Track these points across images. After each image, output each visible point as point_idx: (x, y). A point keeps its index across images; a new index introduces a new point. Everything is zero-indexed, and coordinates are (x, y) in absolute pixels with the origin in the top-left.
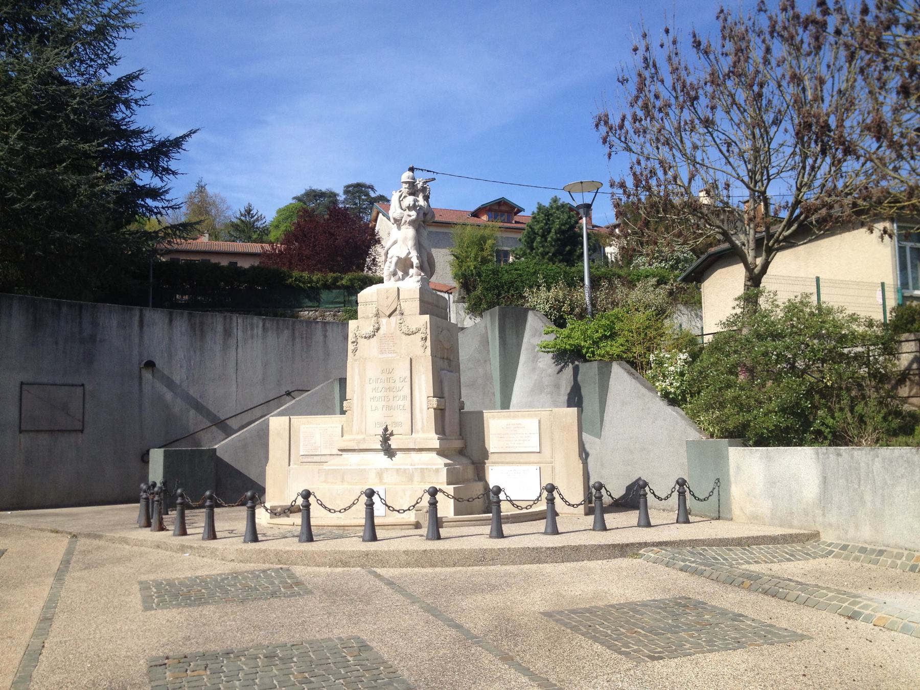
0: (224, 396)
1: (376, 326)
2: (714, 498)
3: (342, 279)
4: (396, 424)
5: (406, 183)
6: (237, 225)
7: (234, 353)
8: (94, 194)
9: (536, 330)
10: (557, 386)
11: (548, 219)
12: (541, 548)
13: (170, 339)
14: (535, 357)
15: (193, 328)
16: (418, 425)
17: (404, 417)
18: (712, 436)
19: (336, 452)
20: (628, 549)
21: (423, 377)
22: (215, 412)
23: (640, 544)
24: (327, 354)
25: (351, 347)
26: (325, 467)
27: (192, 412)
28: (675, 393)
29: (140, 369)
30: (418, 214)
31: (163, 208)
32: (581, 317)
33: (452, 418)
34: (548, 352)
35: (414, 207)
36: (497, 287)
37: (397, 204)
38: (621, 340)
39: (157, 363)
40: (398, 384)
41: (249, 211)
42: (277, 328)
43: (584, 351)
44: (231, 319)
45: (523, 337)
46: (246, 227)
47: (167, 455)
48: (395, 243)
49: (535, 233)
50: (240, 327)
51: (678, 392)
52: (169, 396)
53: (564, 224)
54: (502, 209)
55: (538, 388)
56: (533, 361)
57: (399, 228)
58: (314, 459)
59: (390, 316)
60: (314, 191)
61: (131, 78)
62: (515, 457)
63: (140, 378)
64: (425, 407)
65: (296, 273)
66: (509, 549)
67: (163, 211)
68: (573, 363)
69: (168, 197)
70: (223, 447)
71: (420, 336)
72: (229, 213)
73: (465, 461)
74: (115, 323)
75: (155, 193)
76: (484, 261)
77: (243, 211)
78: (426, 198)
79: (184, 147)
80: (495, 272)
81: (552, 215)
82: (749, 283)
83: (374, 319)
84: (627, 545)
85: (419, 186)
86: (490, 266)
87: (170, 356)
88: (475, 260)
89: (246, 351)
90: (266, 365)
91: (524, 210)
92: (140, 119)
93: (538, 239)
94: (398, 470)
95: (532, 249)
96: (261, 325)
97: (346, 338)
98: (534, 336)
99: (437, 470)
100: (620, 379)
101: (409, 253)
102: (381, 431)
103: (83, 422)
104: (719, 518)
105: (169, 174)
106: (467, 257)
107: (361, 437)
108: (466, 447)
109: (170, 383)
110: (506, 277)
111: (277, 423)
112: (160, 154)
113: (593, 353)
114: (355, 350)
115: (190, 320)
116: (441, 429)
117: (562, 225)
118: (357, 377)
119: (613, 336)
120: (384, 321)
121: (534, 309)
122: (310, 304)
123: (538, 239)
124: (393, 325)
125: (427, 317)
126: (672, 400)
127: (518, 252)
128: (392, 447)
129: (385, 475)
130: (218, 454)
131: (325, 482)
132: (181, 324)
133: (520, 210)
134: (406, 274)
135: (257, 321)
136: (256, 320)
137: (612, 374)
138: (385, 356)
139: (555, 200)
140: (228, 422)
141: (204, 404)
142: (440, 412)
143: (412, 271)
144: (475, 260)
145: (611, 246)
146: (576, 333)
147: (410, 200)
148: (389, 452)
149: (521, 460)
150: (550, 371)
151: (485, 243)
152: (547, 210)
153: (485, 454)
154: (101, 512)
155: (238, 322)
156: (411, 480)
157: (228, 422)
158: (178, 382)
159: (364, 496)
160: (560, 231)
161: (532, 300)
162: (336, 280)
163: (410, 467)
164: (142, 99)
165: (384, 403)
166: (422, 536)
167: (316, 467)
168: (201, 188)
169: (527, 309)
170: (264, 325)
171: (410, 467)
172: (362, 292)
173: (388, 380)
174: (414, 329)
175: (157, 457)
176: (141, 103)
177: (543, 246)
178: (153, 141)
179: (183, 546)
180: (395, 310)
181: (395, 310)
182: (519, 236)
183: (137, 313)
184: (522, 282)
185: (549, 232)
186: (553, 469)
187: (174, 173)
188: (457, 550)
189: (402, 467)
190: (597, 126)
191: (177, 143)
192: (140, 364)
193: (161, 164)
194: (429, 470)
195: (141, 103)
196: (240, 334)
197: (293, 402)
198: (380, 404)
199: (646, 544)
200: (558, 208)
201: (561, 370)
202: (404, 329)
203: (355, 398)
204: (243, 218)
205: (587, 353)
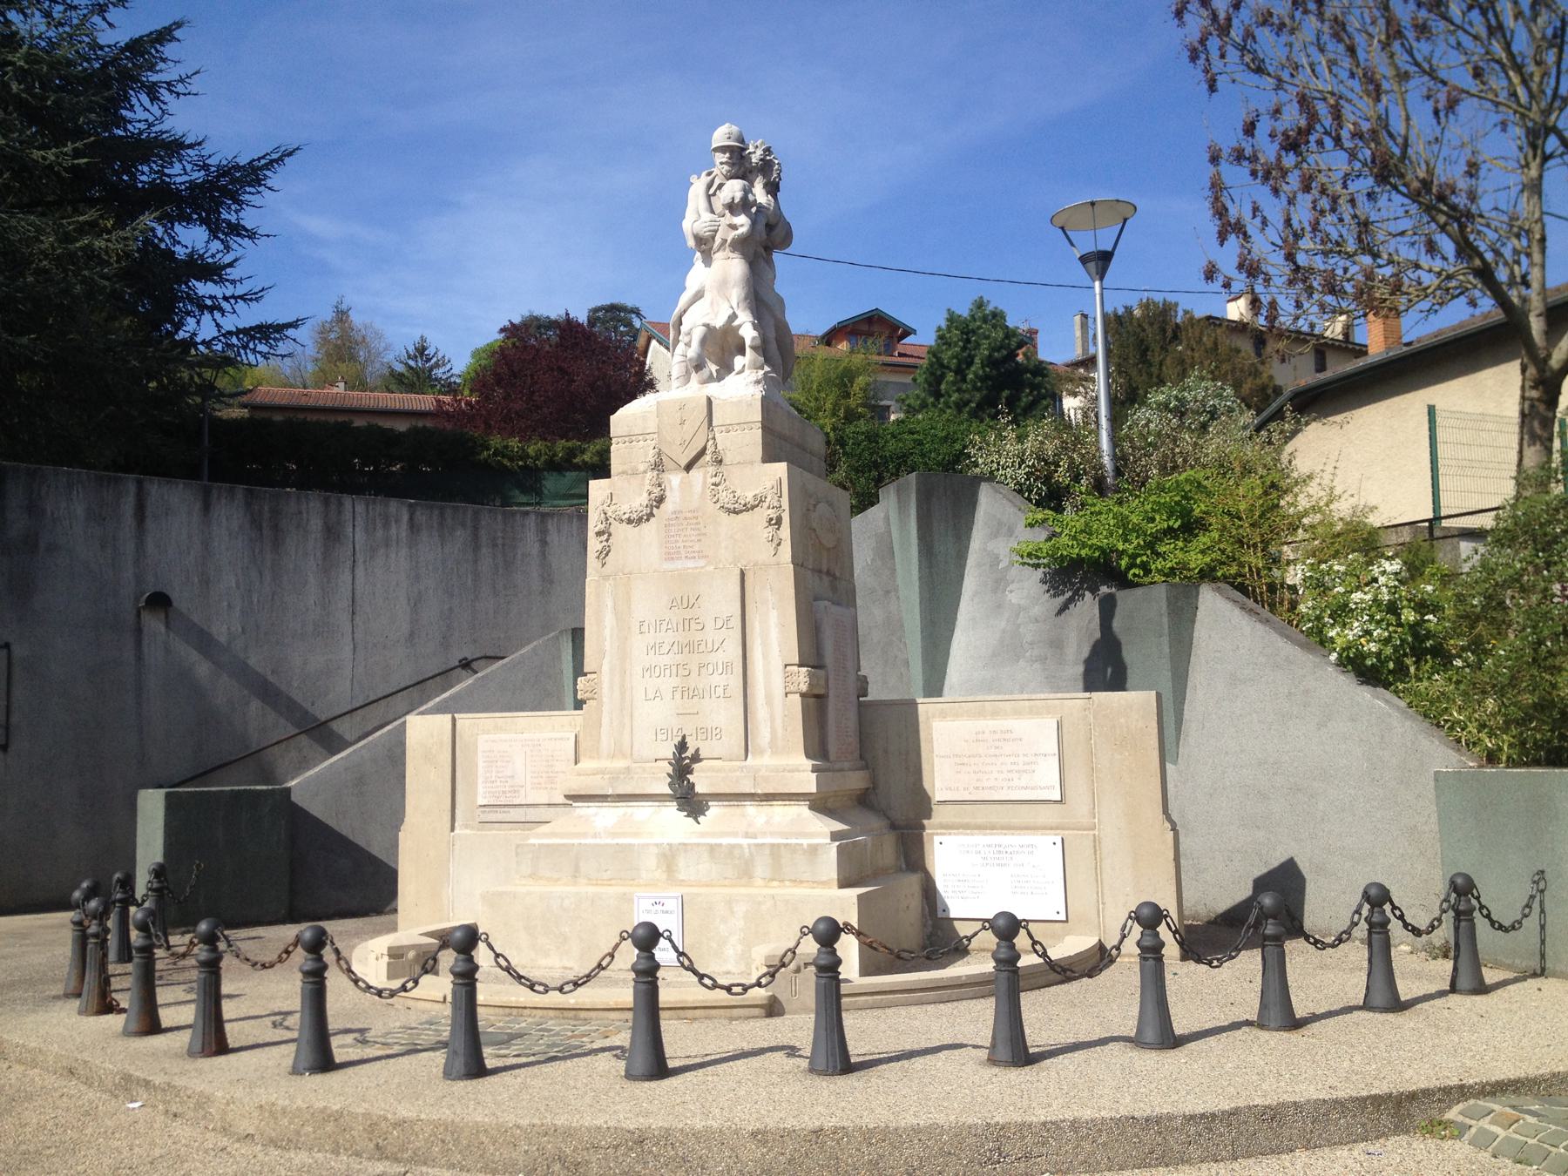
0: (327, 670)
1: (657, 491)
2: (1532, 923)
3: (583, 452)
4: (706, 733)
5: (723, 149)
6: (401, 375)
7: (347, 577)
8: (71, 256)
9: (1000, 524)
10: (1057, 644)
11: (968, 341)
12: (1171, 1117)
13: (206, 544)
14: (998, 581)
15: (256, 523)
16: (763, 734)
17: (725, 716)
18: (1492, 758)
19: (562, 800)
20: (1414, 1109)
21: (773, 616)
22: (307, 705)
23: (1447, 1091)
24: (548, 579)
25: (594, 545)
26: (536, 838)
27: (255, 705)
28: (1378, 654)
29: (138, 615)
30: (754, 223)
31: (225, 298)
32: (1099, 487)
33: (842, 720)
34: (1036, 566)
35: (742, 205)
36: (876, 465)
37: (703, 203)
38: (1204, 540)
39: (175, 596)
40: (711, 635)
41: (421, 350)
42: (441, 525)
43: (1123, 563)
44: (340, 504)
45: (969, 538)
46: (419, 372)
47: (172, 805)
48: (699, 296)
49: (942, 366)
50: (359, 521)
51: (1389, 650)
52: (203, 669)
53: (999, 349)
54: (875, 328)
55: (1009, 650)
56: (995, 591)
57: (708, 261)
58: (510, 815)
59: (688, 468)
60: (537, 318)
61: (164, 35)
62: (997, 814)
63: (139, 630)
64: (779, 691)
65: (496, 441)
66: (1075, 1125)
67: (225, 305)
68: (1094, 590)
69: (233, 273)
70: (311, 782)
71: (763, 513)
72: (389, 357)
73: (876, 823)
74: (80, 510)
75: (213, 272)
76: (851, 416)
77: (411, 350)
78: (773, 188)
79: (269, 183)
80: (872, 437)
81: (973, 332)
82: (1534, 394)
83: (649, 475)
84: (1412, 1096)
85: (755, 159)
86: (862, 426)
87: (206, 582)
88: (834, 414)
89: (383, 571)
90: (416, 603)
91: (914, 332)
92: (180, 119)
93: (950, 377)
94: (712, 849)
95: (938, 395)
96: (405, 518)
97: (583, 518)
98: (994, 535)
99: (814, 850)
100: (1219, 619)
101: (734, 317)
102: (669, 751)
103: (7, 728)
104: (1541, 973)
105: (243, 237)
106: (819, 409)
107: (620, 764)
108: (874, 781)
109: (204, 642)
110: (892, 445)
111: (424, 730)
112: (222, 192)
113: (1145, 568)
114: (605, 553)
115: (248, 505)
116: (817, 746)
117: (994, 350)
118: (609, 620)
119: (1190, 527)
120: (674, 480)
121: (991, 477)
122: (524, 499)
123: (950, 377)
124: (698, 488)
125: (781, 468)
126: (1366, 671)
127: (911, 401)
128: (699, 789)
129: (681, 862)
130: (293, 798)
131: (533, 876)
132: (230, 514)
133: (908, 332)
134: (726, 368)
135: (398, 509)
136: (394, 505)
137: (1200, 614)
138: (679, 565)
139: (980, 305)
140: (335, 725)
141: (283, 688)
142: (816, 705)
143: (739, 361)
144: (834, 414)
145: (1075, 395)
146: (1091, 525)
147: (734, 189)
148: (691, 802)
149: (1015, 821)
150: (1036, 610)
151: (852, 383)
152: (966, 323)
153: (922, 805)
154: (23, 935)
155: (355, 510)
156: (746, 874)
157: (335, 725)
158: (223, 639)
159: (628, 945)
160: (990, 362)
161: (983, 462)
162: (571, 453)
163: (744, 842)
164: (182, 80)
165: (675, 681)
166: (792, 1051)
167: (516, 834)
168: (342, 315)
169: (979, 479)
170: (411, 519)
171: (744, 842)
172: (622, 412)
173: (686, 623)
174: (749, 496)
175: (151, 806)
176: (180, 88)
177: (959, 390)
178: (205, 167)
179: (127, 1078)
180: (702, 452)
181: (702, 452)
182: (908, 379)
183: (132, 488)
184: (923, 455)
185: (970, 363)
186: (1096, 841)
187: (252, 235)
188: (917, 1130)
189: (725, 841)
190: (1179, 14)
191: (252, 175)
192: (137, 600)
193: (225, 215)
194: (793, 849)
195: (180, 88)
196: (360, 536)
197: (470, 681)
198: (668, 683)
199: (1462, 1092)
200: (985, 320)
201: (1064, 608)
202: (725, 497)
203: (605, 668)
204: (412, 363)
205: (1131, 566)
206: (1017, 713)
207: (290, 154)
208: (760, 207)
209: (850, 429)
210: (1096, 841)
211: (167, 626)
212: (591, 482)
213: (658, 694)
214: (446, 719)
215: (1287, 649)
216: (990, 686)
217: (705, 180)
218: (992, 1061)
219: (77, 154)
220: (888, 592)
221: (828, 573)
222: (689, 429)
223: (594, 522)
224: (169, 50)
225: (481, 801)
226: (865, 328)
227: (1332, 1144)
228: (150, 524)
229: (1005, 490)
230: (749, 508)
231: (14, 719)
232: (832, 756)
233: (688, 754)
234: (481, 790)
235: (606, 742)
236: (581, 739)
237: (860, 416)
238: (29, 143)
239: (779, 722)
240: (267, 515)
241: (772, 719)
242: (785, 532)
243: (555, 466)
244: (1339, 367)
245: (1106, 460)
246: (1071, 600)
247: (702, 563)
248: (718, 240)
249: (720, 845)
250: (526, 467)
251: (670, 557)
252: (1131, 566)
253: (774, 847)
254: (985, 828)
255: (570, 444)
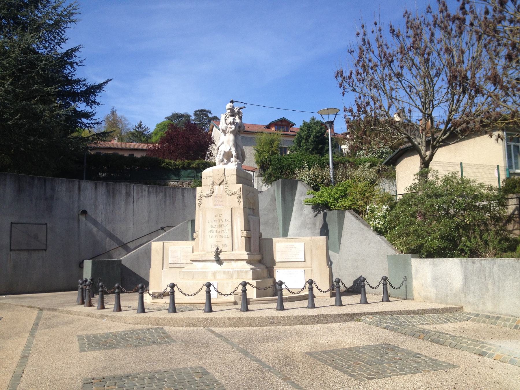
0: (126, 230)
1: (212, 190)
2: (403, 287)
3: (193, 164)
4: (223, 246)
7: (132, 205)
8: (53, 116)
10: (314, 224)
11: (309, 130)
12: (306, 316)
14: (302, 208)
15: (108, 191)
16: (236, 246)
17: (227, 242)
20: (354, 317)
21: (239, 219)
22: (121, 239)
23: (361, 313)
24: (184, 206)
25: (198, 202)
26: (183, 270)
27: (108, 239)
28: (381, 228)
30: (236, 127)
31: (92, 124)
32: (328, 185)
33: (255, 243)
34: (309, 205)
35: (233, 123)
37: (224, 122)
39: (88, 211)
40: (225, 223)
41: (140, 125)
42: (156, 192)
43: (329, 205)
44: (130, 186)
46: (139, 134)
47: (93, 264)
48: (223, 143)
49: (301, 137)
50: (135, 191)
52: (95, 230)
53: (318, 133)
54: (283, 124)
55: (303, 225)
56: (301, 210)
57: (225, 135)
58: (177, 266)
59: (220, 185)
60: (177, 114)
61: (74, 50)
62: (290, 264)
63: (79, 220)
65: (167, 161)
66: (287, 317)
67: (92, 126)
69: (94, 117)
70: (125, 258)
71: (236, 196)
73: (262, 266)
74: (64, 189)
75: (87, 115)
76: (273, 153)
78: (240, 118)
80: (279, 160)
81: (311, 127)
82: (422, 166)
84: (354, 314)
85: (236, 111)
86: (276, 156)
87: (96, 207)
89: (139, 204)
93: (304, 141)
94: (224, 272)
95: (300, 146)
96: (147, 190)
97: (195, 197)
98: (301, 195)
99: (247, 272)
101: (231, 149)
102: (215, 250)
104: (406, 299)
105: (95, 104)
106: (263, 151)
107: (203, 253)
109: (95, 223)
110: (285, 162)
111: (156, 245)
112: (90, 93)
113: (334, 205)
114: (200, 204)
115: (107, 187)
116: (248, 248)
118: (201, 219)
119: (346, 196)
120: (216, 187)
121: (301, 180)
122: (175, 178)
123: (304, 141)
124: (222, 189)
125: (241, 185)
127: (292, 148)
128: (221, 259)
129: (217, 275)
131: (183, 278)
132: (102, 190)
133: (293, 125)
134: (229, 161)
136: (144, 187)
138: (217, 207)
139: (313, 119)
140: (128, 245)
141: (115, 235)
142: (248, 240)
144: (268, 153)
145: (344, 145)
146: (325, 194)
147: (231, 119)
148: (219, 261)
149: (294, 266)
151: (273, 143)
152: (309, 124)
153: (273, 263)
154: (56, 296)
155: (134, 188)
156: (232, 277)
157: (128, 245)
158: (100, 222)
160: (316, 136)
161: (300, 175)
162: (189, 164)
163: (231, 270)
164: (80, 62)
166: (238, 309)
168: (113, 113)
169: (298, 181)
170: (148, 190)
174: (233, 192)
175: (88, 265)
176: (80, 64)
177: (306, 145)
178: (86, 86)
180: (223, 181)
181: (223, 181)
182: (293, 139)
183: (77, 183)
184: (295, 165)
185: (310, 137)
186: (312, 271)
187: (98, 104)
188: (258, 317)
189: (227, 270)
190: (336, 77)
191: (100, 87)
192: (78, 212)
193: (91, 99)
194: (242, 272)
195: (80, 64)
197: (165, 233)
198: (214, 234)
200: (314, 124)
201: (316, 215)
202: (228, 192)
204: (137, 129)
205: (331, 205)
206: (295, 241)
207: (110, 81)
208: (237, 123)
209: (273, 157)
210: (312, 271)
211: (86, 219)
213: (212, 237)
214: (161, 243)
215: (363, 226)
216: (298, 235)
217: (224, 116)
218: (277, 310)
219: (56, 88)
220: (274, 210)
221: (252, 209)
222: (220, 176)
223: (198, 197)
224: (77, 54)
225: (170, 262)
226: (280, 123)
227: (337, 322)
228: (82, 192)
229: (304, 183)
230: (233, 194)
231: (48, 242)
232: (252, 251)
233: (219, 250)
235: (200, 248)
236: (194, 249)
237: (276, 153)
238: (44, 87)
239: (240, 244)
240: (111, 189)
242: (241, 200)
243: (184, 168)
245: (331, 175)
246: (318, 213)
247: (222, 207)
248: (227, 131)
250: (176, 168)
251: (215, 205)
252: (331, 205)
253: (238, 272)
254: (289, 268)
255: (189, 161)
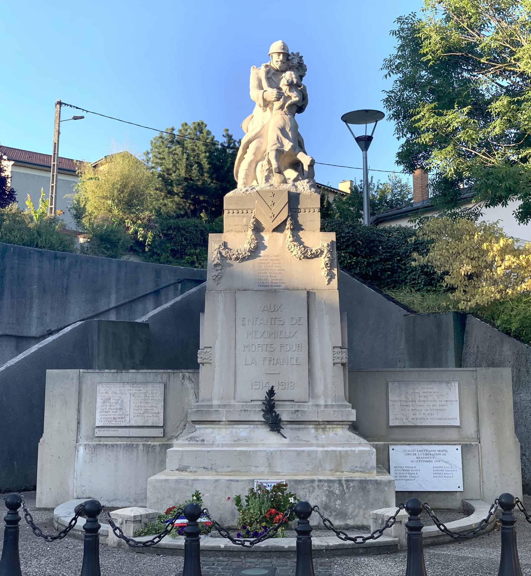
102: (262, 395)
148: (274, 423)
212: (210, 234)
225: (97, 425)
234: (98, 416)
241: (325, 379)
244: (395, 211)
249: (303, 451)
